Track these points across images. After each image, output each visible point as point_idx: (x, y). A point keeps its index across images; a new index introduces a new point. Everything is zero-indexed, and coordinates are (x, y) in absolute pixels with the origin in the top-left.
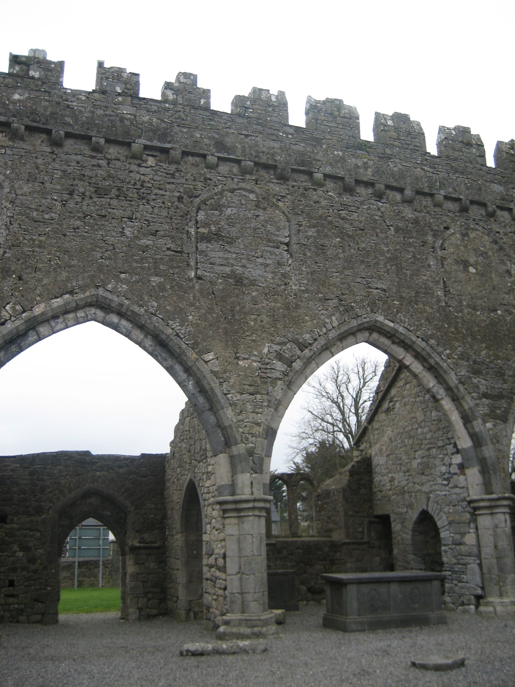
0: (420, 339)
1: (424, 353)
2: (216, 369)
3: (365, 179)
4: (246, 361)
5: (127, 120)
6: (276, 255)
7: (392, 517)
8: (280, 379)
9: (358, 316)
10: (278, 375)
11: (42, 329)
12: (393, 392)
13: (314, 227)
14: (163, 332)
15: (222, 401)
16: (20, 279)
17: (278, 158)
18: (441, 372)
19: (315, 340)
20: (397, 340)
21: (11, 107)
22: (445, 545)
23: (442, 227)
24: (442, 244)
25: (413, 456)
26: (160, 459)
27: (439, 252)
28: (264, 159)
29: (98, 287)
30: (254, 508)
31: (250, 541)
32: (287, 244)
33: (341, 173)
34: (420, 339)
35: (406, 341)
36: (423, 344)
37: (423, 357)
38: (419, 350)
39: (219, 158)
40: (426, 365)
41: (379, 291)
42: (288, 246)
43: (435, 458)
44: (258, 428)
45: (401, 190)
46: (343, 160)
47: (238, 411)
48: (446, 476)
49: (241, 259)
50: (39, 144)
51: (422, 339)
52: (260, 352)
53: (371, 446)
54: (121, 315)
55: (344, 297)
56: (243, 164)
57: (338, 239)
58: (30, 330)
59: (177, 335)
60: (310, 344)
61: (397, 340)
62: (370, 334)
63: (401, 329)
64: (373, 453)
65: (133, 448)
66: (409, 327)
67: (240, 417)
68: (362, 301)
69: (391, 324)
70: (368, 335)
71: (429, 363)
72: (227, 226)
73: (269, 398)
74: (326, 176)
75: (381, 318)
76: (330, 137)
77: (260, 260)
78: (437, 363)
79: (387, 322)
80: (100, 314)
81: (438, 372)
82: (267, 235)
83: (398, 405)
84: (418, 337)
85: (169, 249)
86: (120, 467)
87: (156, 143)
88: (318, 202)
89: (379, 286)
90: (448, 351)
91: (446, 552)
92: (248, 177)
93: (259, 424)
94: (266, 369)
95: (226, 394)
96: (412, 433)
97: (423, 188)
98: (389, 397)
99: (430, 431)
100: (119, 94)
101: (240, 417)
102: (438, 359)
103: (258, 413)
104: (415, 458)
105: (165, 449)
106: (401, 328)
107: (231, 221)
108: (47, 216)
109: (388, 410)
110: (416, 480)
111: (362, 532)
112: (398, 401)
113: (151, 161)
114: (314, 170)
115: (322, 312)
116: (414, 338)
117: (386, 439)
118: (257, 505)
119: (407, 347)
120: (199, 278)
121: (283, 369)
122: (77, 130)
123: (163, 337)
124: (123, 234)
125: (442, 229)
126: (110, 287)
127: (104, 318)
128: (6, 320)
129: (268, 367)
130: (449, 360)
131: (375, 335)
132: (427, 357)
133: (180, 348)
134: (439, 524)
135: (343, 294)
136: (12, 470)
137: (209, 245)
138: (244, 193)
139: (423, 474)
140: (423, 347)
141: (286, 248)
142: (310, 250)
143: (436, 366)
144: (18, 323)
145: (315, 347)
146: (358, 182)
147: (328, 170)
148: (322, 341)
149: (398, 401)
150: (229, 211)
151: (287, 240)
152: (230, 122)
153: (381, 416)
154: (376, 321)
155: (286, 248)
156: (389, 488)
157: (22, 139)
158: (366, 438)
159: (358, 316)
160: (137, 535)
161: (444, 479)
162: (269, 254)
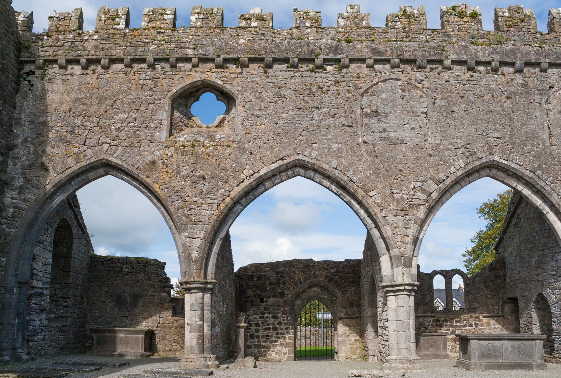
0: (528, 171)
1: (531, 181)
2: (378, 201)
3: (484, 59)
4: (398, 195)
5: (311, 43)
6: (418, 121)
7: (520, 298)
8: (422, 205)
9: (480, 159)
10: (421, 202)
11: (267, 184)
12: (519, 211)
13: (445, 99)
14: (342, 179)
15: (382, 221)
16: (251, 153)
17: (417, 53)
18: (546, 194)
19: (448, 177)
20: (511, 173)
21: (239, 48)
22: (554, 317)
23: (547, 87)
24: (547, 100)
25: (532, 256)
26: (358, 262)
27: (544, 106)
28: (406, 56)
29: (299, 154)
30: (405, 290)
31: (402, 311)
32: (426, 113)
33: (464, 58)
34: (528, 171)
35: (518, 173)
36: (531, 175)
37: (531, 184)
38: (528, 179)
39: (375, 60)
40: (534, 190)
41: (495, 139)
42: (427, 115)
43: (547, 256)
44: (407, 238)
45: (512, 64)
46: (465, 48)
47: (394, 228)
48: (555, 269)
49: (393, 127)
50: (233, 68)
51: (530, 171)
52: (407, 188)
53: (505, 250)
54: (315, 171)
55: (469, 145)
56: (392, 61)
57: (464, 106)
58: (259, 184)
59: (351, 180)
60: (444, 180)
61: (511, 173)
62: (490, 170)
63: (513, 165)
64: (507, 255)
65: (339, 257)
66: (519, 163)
67: (395, 232)
68: (483, 147)
69: (506, 162)
70: (489, 171)
71: (536, 188)
72: (382, 105)
73: (414, 217)
74: (454, 62)
75: (497, 159)
76: (459, 33)
77: (407, 126)
78: (542, 187)
79: (502, 161)
80: (302, 171)
81: (544, 194)
82: (411, 108)
83: (522, 221)
84: (527, 170)
85: (343, 125)
86: (332, 268)
87: (331, 56)
88: (448, 81)
89: (495, 136)
90: (551, 178)
91: (555, 322)
92: (396, 69)
93: (407, 236)
94: (413, 199)
95: (385, 217)
96: (532, 240)
97: (531, 60)
98: (516, 215)
99: (544, 237)
100: (308, 28)
101: (395, 232)
102: (543, 184)
103: (408, 228)
104: (534, 257)
105: (360, 256)
106: (513, 164)
107: (385, 102)
108: (265, 113)
109: (516, 224)
110: (534, 272)
111: (499, 309)
112: (522, 217)
113: (329, 68)
114: (443, 58)
115: (453, 157)
116: (524, 171)
117: (514, 244)
118: (407, 287)
119: (519, 178)
120: (365, 142)
121: (424, 198)
122: (279, 56)
123: (342, 182)
124: (313, 119)
125: (548, 88)
126: (306, 153)
127: (305, 173)
128: (244, 180)
129: (414, 197)
130: (552, 185)
131: (494, 171)
132: (534, 184)
133: (353, 189)
134: (550, 302)
135: (468, 144)
136: (266, 271)
137: (371, 120)
138: (393, 81)
139: (539, 268)
140: (531, 176)
141: (425, 116)
142: (442, 115)
143: (541, 190)
144: (251, 181)
145: (448, 181)
146: (478, 63)
147: (454, 57)
148: (453, 178)
149: (522, 217)
150: (384, 96)
151: (426, 110)
152: (385, 33)
153: (511, 229)
154: (493, 161)
155: (425, 116)
156: (516, 278)
157: (248, 67)
158: (502, 245)
159: (480, 159)
160: (343, 310)
161: (554, 271)
162: (412, 121)
